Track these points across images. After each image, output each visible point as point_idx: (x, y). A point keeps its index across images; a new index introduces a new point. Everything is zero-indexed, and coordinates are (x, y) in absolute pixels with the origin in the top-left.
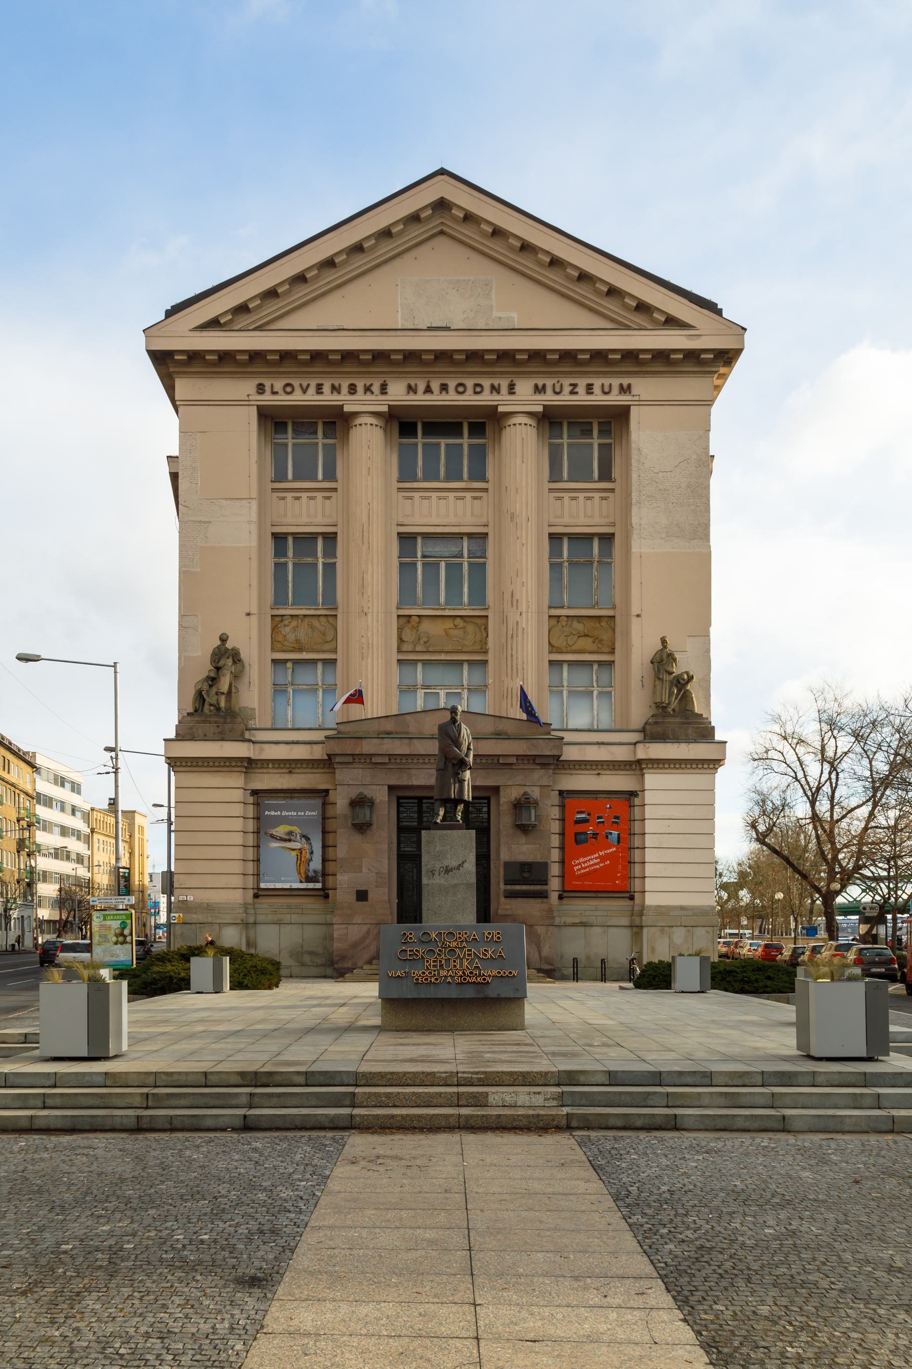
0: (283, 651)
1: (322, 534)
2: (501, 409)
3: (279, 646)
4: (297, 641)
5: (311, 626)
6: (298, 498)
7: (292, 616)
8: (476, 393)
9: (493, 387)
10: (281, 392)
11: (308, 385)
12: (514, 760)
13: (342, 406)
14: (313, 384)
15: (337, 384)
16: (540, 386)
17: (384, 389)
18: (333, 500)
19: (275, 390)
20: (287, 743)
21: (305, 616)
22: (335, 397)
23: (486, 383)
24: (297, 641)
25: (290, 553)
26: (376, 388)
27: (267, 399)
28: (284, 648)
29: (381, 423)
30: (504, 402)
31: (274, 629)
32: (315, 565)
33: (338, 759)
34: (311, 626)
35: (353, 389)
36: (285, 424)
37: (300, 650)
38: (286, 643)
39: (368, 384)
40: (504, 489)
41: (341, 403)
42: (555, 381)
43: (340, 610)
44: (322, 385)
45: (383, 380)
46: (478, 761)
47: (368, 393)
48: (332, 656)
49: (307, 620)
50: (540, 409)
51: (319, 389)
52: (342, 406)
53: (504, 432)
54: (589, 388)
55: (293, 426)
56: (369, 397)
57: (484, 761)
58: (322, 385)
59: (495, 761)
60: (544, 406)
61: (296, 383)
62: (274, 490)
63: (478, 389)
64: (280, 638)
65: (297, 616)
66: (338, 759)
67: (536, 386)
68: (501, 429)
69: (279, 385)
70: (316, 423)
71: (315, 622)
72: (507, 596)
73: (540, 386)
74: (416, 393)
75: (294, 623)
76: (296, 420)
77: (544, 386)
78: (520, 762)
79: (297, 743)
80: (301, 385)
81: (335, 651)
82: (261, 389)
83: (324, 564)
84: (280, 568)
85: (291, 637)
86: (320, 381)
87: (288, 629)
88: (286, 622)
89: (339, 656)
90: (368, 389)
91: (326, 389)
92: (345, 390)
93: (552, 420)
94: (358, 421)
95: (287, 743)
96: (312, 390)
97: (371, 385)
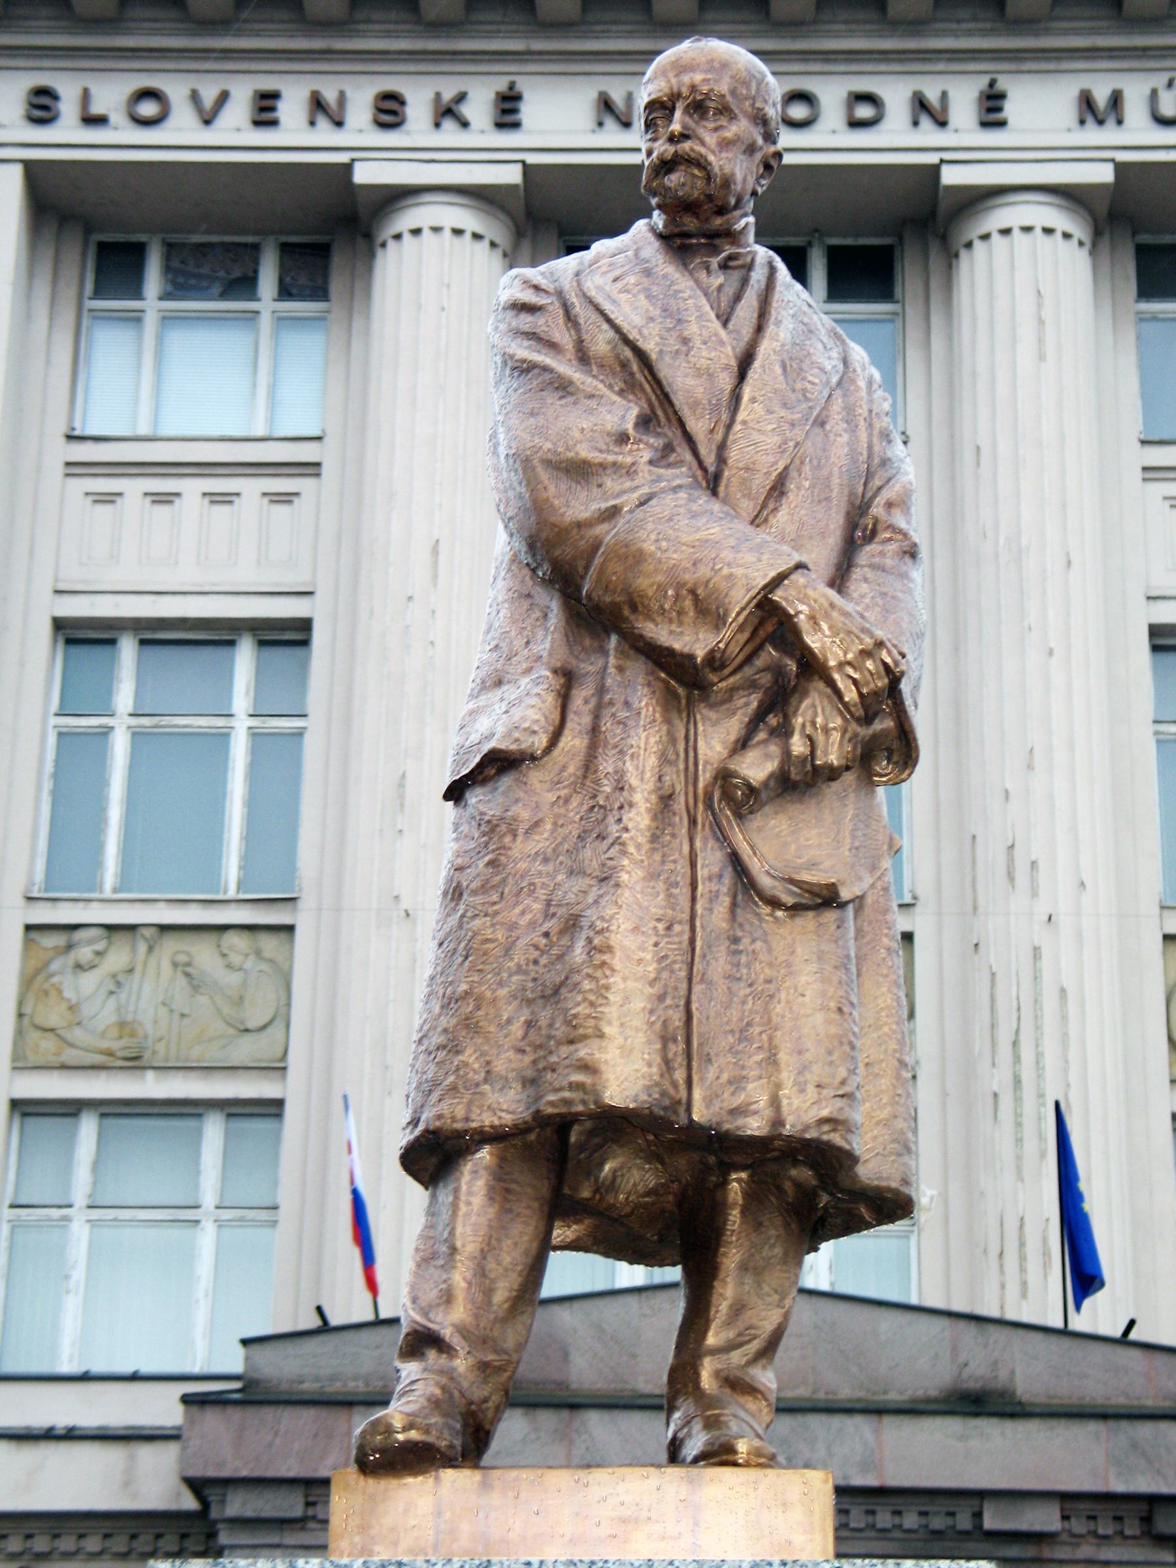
0: (64, 1067)
1: (136, 625)
2: (951, 176)
3: (48, 1044)
4: (124, 1027)
5: (185, 968)
6: (164, 499)
7: (111, 928)
8: (856, 124)
9: (921, 105)
10: (118, 117)
11: (224, 97)
12: (1046, 1519)
13: (348, 168)
14: (242, 93)
15: (330, 96)
16: (1101, 97)
17: (507, 111)
18: (303, 505)
19: (96, 109)
20: (103, 1436)
21: (164, 928)
22: (324, 135)
23: (896, 94)
24: (124, 1027)
25: (241, 700)
26: (479, 108)
27: (66, 138)
28: (71, 1056)
29: (494, 228)
30: (962, 152)
31: (33, 982)
32: (223, 738)
33: (237, 1505)
34: (185, 968)
35: (390, 112)
36: (134, 255)
37: (134, 1063)
38: (77, 1035)
39: (448, 96)
40: (968, 456)
41: (932, 159)
42: (192, 82)
43: (307, 903)
44: (275, 96)
45: (983, 81)
46: (857, 1519)
47: (449, 124)
48: (265, 1089)
49: (171, 946)
50: (1104, 174)
51: (265, 109)
52: (348, 168)
53: (380, 253)
54: (265, 109)
55: (167, 259)
56: (450, 135)
57: (911, 1520)
58: (275, 96)
59: (964, 1522)
60: (527, 168)
61: (176, 89)
62: (74, 468)
63: (864, 112)
64: (54, 1016)
65: (132, 928)
66: (237, 1505)
67: (1087, 102)
68: (951, 257)
69: (111, 94)
70: (256, 247)
71: (203, 953)
72: (991, 854)
73: (1101, 97)
74: (339, 124)
75: (118, 957)
76: (174, 238)
77: (1116, 100)
78: (1078, 1526)
79: (71, 1435)
80: (195, 97)
81: (279, 1069)
82: (42, 108)
83: (255, 735)
84: (79, 754)
85: (103, 1014)
86: (268, 84)
87: (88, 981)
88: (85, 953)
89: (292, 1090)
90: (448, 112)
91: (292, 107)
92: (360, 111)
93: (1146, 238)
94: (406, 220)
95: (103, 1436)
96: (238, 111)
97: (461, 97)
